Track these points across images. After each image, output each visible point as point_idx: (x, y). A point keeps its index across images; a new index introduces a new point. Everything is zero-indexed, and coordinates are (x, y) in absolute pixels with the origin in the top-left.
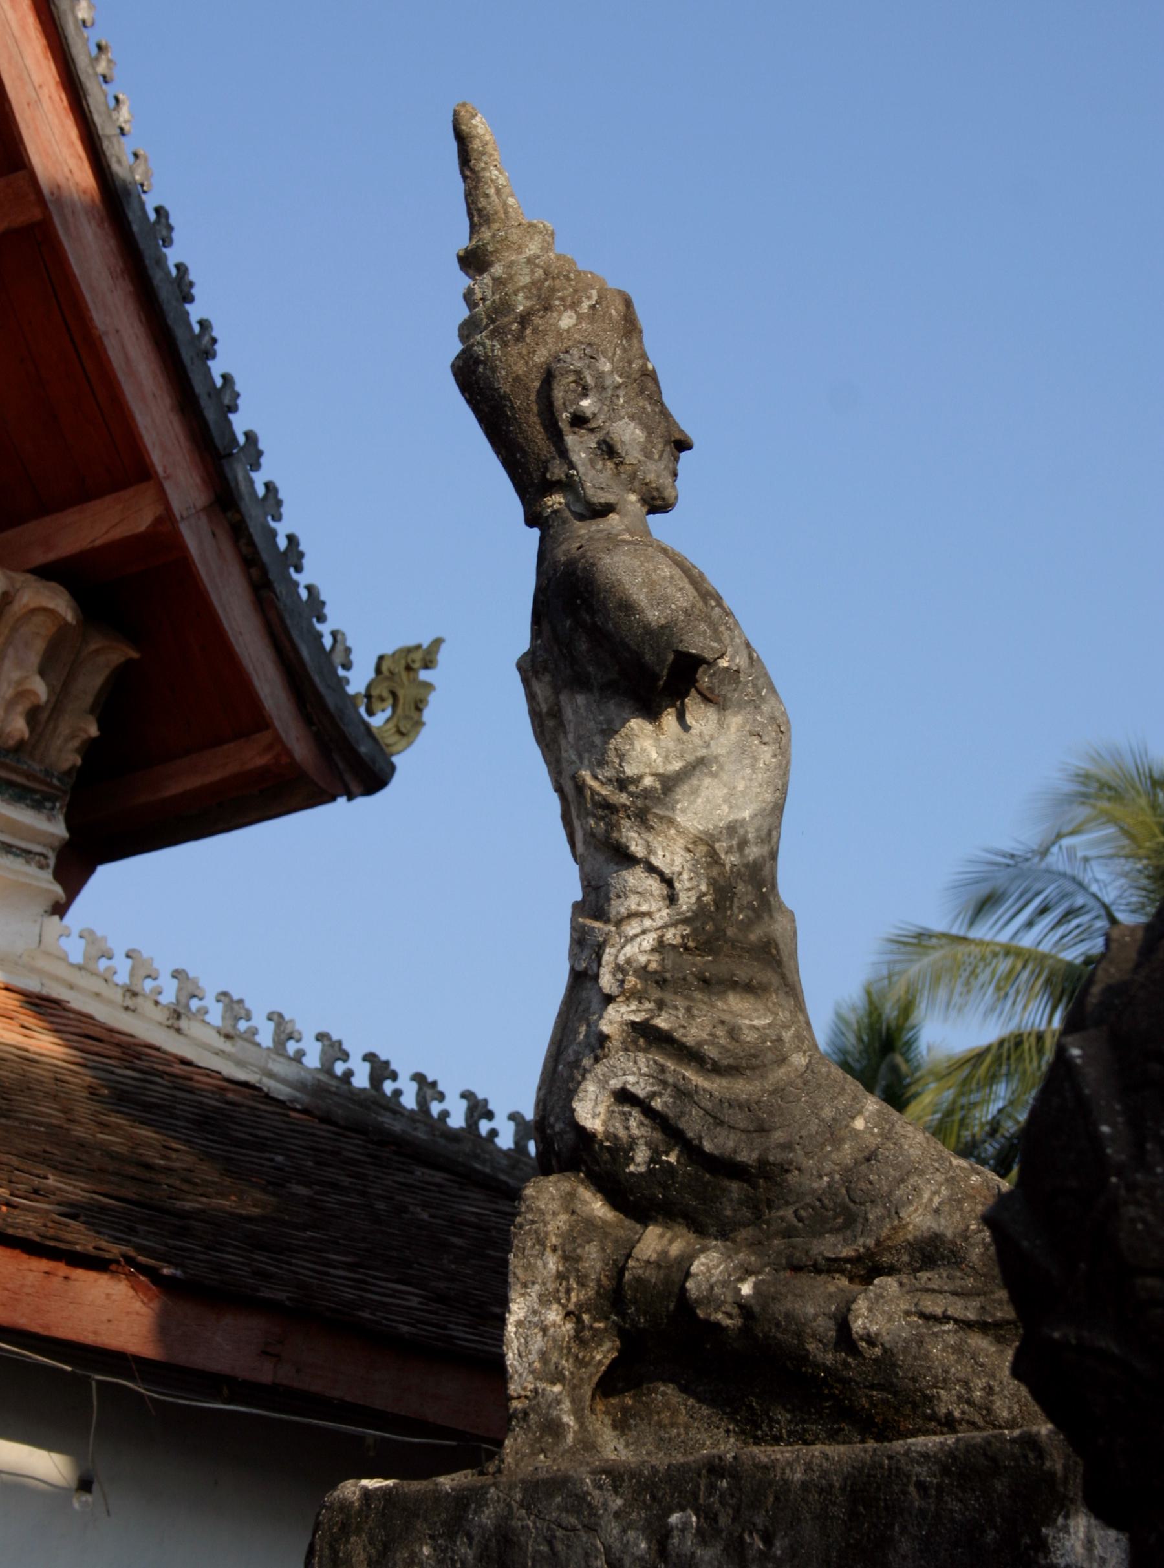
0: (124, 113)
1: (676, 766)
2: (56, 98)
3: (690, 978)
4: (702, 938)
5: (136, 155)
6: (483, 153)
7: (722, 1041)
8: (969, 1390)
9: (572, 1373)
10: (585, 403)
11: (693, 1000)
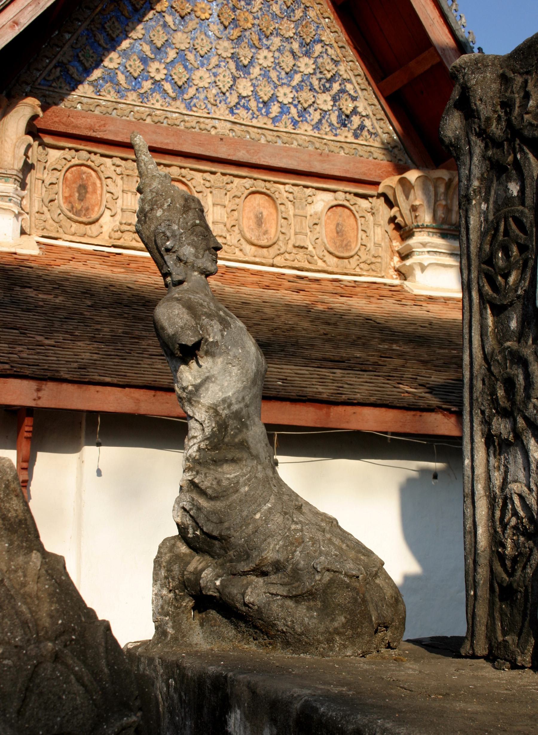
0: (463, 20)
1: (199, 381)
2: (439, 21)
3: (209, 461)
4: (213, 444)
5: (469, 33)
6: (139, 150)
7: (214, 486)
8: (286, 621)
9: (173, 612)
10: (168, 243)
11: (209, 469)
